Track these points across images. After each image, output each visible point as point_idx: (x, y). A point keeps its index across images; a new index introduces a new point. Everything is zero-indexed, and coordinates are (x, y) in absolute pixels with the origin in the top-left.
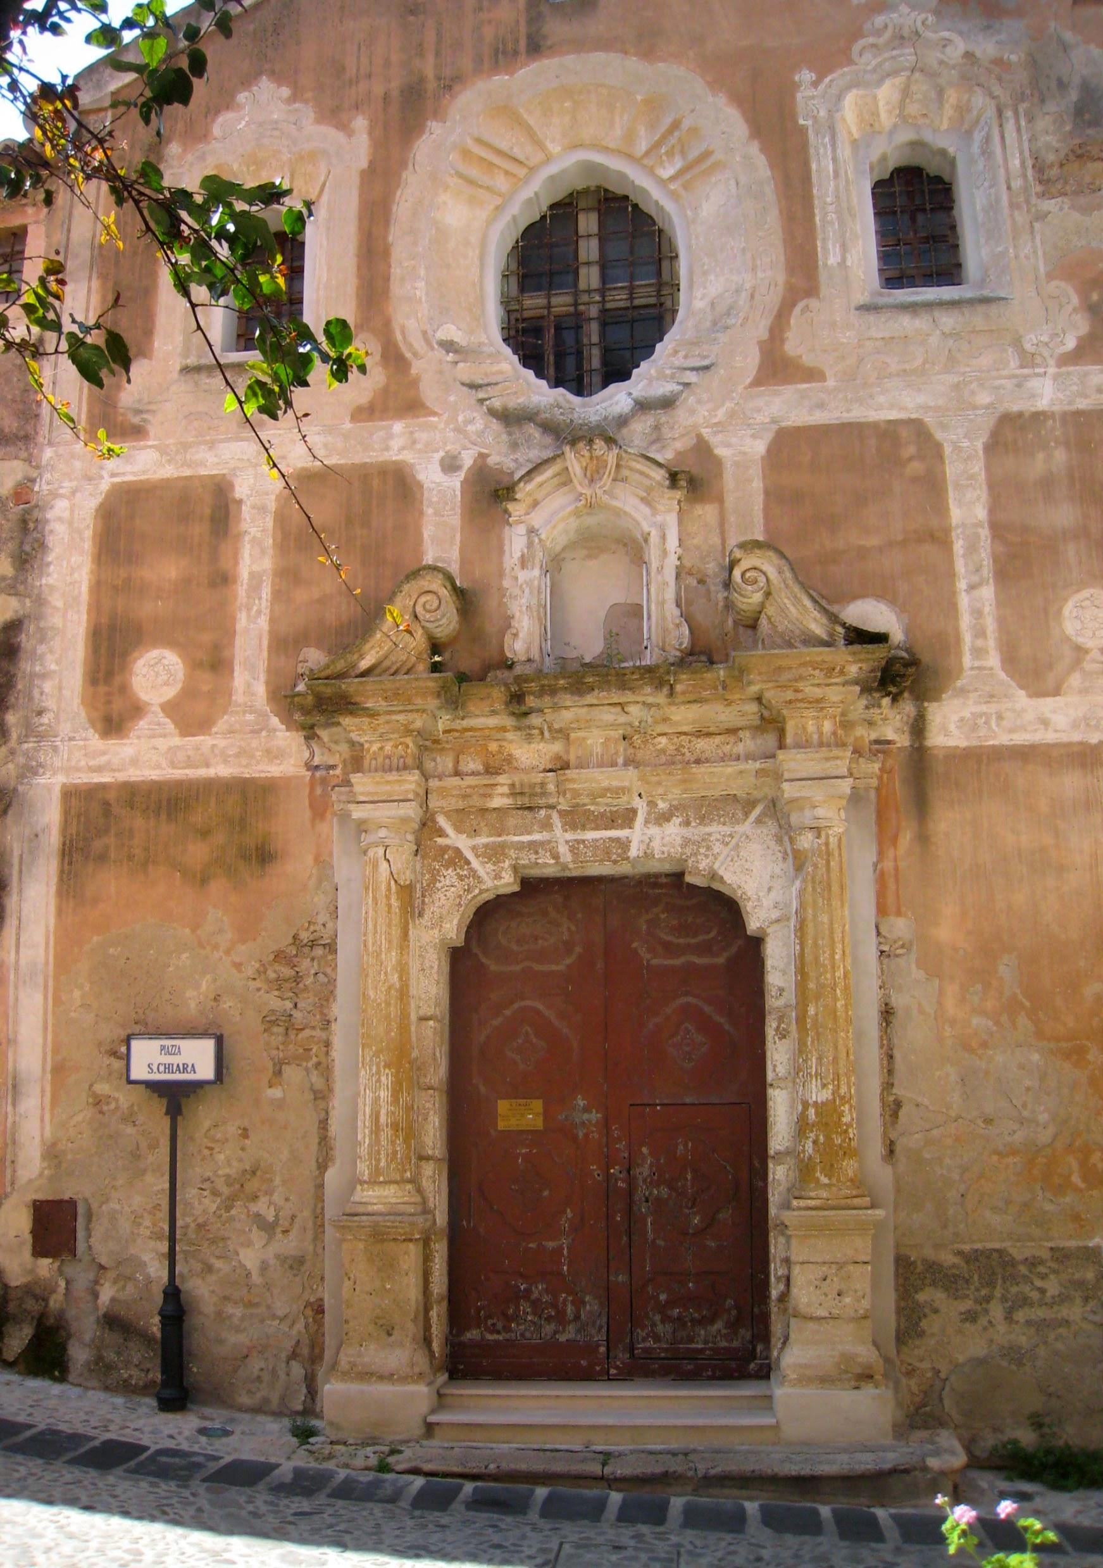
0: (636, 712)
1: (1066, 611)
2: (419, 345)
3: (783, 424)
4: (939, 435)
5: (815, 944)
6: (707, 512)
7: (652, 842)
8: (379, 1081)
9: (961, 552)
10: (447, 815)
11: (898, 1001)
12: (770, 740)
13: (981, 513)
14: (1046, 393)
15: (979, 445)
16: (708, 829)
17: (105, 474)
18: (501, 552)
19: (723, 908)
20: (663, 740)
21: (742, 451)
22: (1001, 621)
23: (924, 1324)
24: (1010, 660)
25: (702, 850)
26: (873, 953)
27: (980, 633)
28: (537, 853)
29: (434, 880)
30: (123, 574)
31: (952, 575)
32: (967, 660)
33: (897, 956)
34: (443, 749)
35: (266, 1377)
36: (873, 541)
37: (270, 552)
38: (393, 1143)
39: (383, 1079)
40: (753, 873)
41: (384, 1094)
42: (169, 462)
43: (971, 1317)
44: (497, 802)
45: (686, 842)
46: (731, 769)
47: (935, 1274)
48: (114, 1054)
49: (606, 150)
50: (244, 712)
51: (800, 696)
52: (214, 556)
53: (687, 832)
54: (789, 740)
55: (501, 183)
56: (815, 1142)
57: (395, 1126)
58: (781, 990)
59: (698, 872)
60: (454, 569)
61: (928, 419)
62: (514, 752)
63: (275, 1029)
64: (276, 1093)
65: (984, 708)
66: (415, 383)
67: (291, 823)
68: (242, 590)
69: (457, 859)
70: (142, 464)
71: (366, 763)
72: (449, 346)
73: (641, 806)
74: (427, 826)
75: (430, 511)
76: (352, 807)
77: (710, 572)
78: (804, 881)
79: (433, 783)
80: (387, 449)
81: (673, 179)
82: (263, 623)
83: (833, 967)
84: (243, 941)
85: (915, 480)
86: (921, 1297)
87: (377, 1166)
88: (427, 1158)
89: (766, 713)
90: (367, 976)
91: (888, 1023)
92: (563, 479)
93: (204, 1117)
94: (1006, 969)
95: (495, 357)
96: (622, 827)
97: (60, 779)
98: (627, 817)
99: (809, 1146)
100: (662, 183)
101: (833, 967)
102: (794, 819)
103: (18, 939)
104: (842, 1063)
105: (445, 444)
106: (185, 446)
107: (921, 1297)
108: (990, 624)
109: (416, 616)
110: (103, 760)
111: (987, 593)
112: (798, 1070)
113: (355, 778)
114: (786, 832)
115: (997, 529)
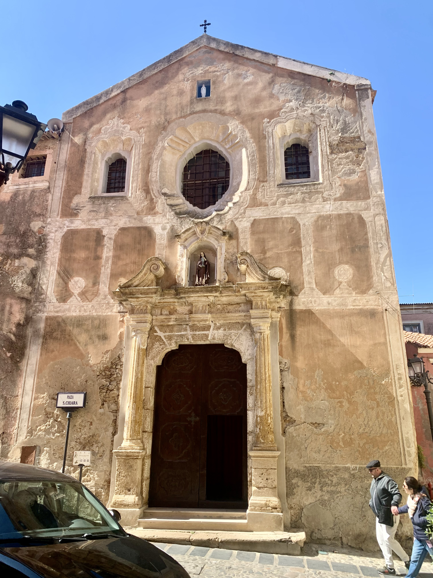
5: (260, 367)
6: (234, 242)
7: (214, 336)
10: (158, 326)
11: (285, 385)
12: (249, 306)
16: (231, 332)
17: (65, 226)
19: (235, 355)
20: (219, 306)
21: (243, 225)
25: (229, 338)
28: (182, 338)
29: (153, 345)
30: (68, 255)
33: (285, 371)
37: (112, 251)
38: (135, 427)
40: (242, 344)
42: (84, 224)
43: (309, 489)
45: (225, 335)
47: (297, 473)
48: (54, 399)
49: (211, 140)
51: (256, 295)
52: (96, 250)
53: (225, 333)
54: (253, 307)
55: (182, 148)
56: (259, 429)
58: (251, 380)
63: (103, 391)
64: (101, 411)
68: (103, 261)
69: (160, 339)
70: (78, 224)
71: (135, 311)
72: (165, 194)
74: (152, 329)
78: (257, 347)
81: (229, 148)
82: (109, 271)
86: (294, 481)
88: (145, 432)
89: (247, 299)
91: (283, 392)
92: (194, 233)
93: (78, 421)
94: (318, 373)
95: (178, 197)
96: (207, 331)
97: (46, 314)
98: (208, 328)
99: (258, 430)
100: (226, 149)
102: (255, 329)
103: (27, 363)
104: (268, 403)
106: (89, 220)
107: (294, 481)
110: (58, 309)
114: (253, 333)
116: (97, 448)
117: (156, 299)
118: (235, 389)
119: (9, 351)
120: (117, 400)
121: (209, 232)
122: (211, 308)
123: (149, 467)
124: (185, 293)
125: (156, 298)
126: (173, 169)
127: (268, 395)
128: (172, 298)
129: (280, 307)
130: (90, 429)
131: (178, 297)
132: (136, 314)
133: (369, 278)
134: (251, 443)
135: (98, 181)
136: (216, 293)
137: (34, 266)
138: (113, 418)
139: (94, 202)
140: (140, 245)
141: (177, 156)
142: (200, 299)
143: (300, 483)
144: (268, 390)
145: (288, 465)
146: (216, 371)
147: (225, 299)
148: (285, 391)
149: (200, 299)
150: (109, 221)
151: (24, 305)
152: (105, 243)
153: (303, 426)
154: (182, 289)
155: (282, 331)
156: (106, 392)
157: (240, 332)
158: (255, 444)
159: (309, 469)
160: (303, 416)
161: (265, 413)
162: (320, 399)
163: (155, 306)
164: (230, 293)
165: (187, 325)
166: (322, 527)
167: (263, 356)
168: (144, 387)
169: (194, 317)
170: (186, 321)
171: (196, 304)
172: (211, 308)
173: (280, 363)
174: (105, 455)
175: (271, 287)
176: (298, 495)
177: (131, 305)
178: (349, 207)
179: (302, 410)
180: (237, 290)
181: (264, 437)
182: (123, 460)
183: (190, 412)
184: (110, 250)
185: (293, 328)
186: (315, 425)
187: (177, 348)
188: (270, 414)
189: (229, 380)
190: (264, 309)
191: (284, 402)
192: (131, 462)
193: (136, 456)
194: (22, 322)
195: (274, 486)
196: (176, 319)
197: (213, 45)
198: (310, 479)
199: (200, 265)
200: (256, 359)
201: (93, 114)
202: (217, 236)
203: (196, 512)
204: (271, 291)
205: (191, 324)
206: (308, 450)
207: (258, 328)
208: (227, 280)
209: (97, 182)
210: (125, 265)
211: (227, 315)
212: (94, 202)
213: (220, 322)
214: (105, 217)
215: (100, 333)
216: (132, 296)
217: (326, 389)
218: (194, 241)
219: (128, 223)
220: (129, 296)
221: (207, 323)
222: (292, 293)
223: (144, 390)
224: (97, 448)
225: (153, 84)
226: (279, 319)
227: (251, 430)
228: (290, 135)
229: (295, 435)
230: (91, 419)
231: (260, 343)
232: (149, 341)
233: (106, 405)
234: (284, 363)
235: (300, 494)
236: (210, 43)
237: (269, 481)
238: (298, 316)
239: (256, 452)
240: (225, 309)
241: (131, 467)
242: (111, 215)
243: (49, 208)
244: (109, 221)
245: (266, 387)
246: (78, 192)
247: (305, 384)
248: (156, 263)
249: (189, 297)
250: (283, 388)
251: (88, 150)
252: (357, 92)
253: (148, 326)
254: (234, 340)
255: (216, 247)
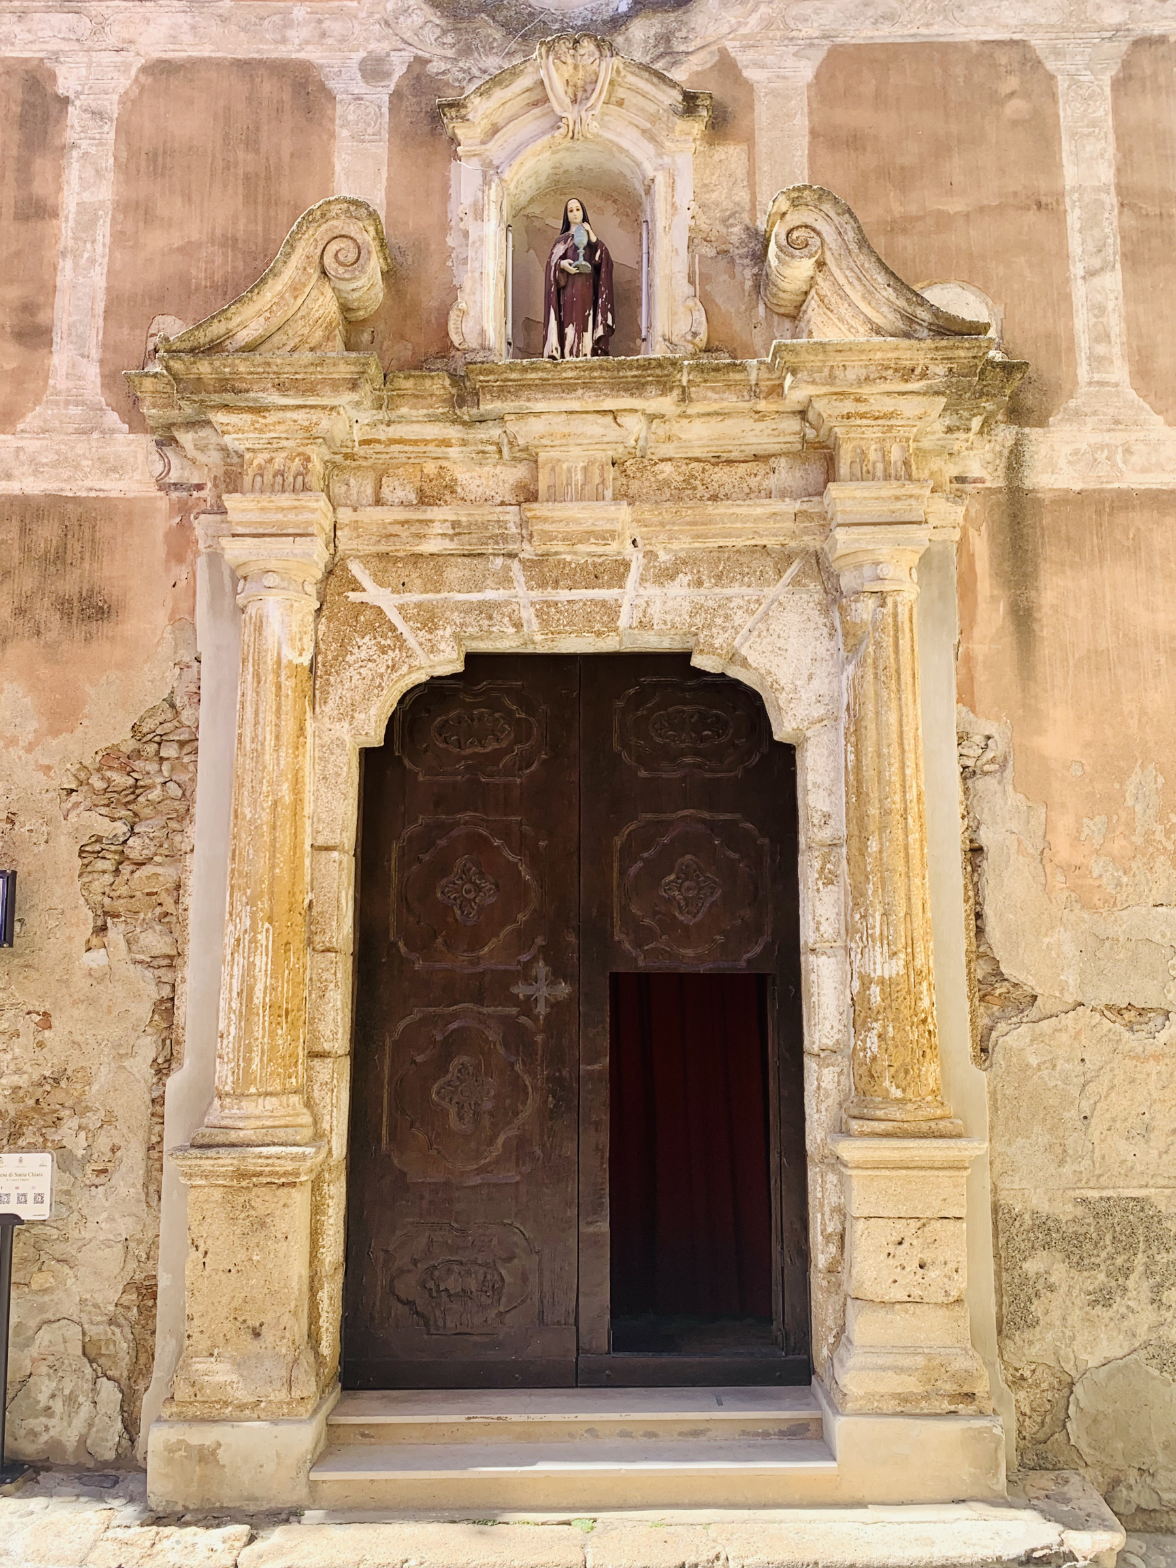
0: (634, 426)
3: (839, 40)
4: (1051, 65)
6: (731, 154)
7: (644, 615)
8: (254, 941)
9: (1077, 226)
10: (365, 559)
11: (985, 838)
12: (815, 472)
13: (1106, 174)
15: (1106, 80)
16: (727, 592)
18: (445, 197)
20: (667, 468)
23: (1037, 1308)
24: (1143, 371)
25: (719, 621)
28: (491, 618)
31: (1063, 256)
33: (986, 774)
34: (359, 467)
35: (58, 1406)
36: (956, 206)
38: (272, 1034)
39: (261, 937)
40: (784, 659)
41: (261, 962)
43: (1102, 1298)
44: (430, 546)
45: (697, 609)
46: (761, 508)
47: (1046, 1232)
50: (67, 403)
51: (862, 408)
53: (699, 595)
54: (844, 469)
59: (712, 650)
60: (378, 199)
61: (1038, 42)
62: (459, 477)
63: (100, 865)
64: (97, 958)
65: (1107, 438)
67: (133, 567)
68: (66, 228)
69: (378, 622)
71: (247, 480)
73: (636, 559)
74: (334, 573)
75: (345, 133)
76: (224, 542)
77: (734, 239)
79: (345, 515)
80: (284, 41)
83: (903, 786)
84: (55, 732)
86: (1030, 1267)
87: (247, 1071)
89: (811, 434)
90: (241, 786)
91: (975, 867)
98: (617, 572)
101: (903, 786)
104: (918, 921)
105: (367, 40)
107: (1030, 1267)
108: (1116, 325)
109: (324, 273)
111: (1113, 281)
112: (850, 930)
113: (231, 501)
114: (835, 597)
116: (82, 1134)
117: (350, 417)
118: (736, 856)
120: (169, 907)
121: (610, 94)
122: (627, 475)
123: (342, 1213)
124: (502, 392)
125: (354, 414)
127: (917, 881)
128: (433, 419)
129: (961, 480)
130: (41, 1045)
131: (466, 413)
132: (252, 490)
134: (830, 1101)
136: (663, 393)
138: (153, 993)
140: (257, 151)
142: (578, 425)
143: (1059, 1273)
144: (916, 862)
145: (1005, 1198)
146: (643, 774)
147: (699, 435)
148: (985, 864)
149: (573, 424)
150: (84, 25)
152: (70, 136)
153: (1070, 1023)
154: (491, 372)
155: (974, 590)
156: (117, 872)
157: (770, 592)
158: (858, 1109)
159: (1102, 1211)
160: (1071, 978)
161: (907, 966)
162: (1151, 903)
163: (344, 461)
164: (731, 401)
165: (511, 555)
166: (1161, 1458)
167: (894, 704)
168: (308, 848)
169: (546, 520)
170: (505, 538)
171: (555, 454)
172: (627, 475)
173: (962, 738)
174: (123, 1169)
175: (941, 370)
176: (1050, 1325)
177: (224, 449)
179: (1070, 950)
180: (765, 386)
182: (217, 1194)
183: (525, 958)
184: (98, 173)
185: (1025, 575)
186: (1127, 1015)
187: (459, 667)
188: (925, 971)
189: (706, 815)
190: (897, 479)
191: (978, 916)
192: (264, 1202)
193: (285, 1174)
195: (954, 1294)
196: (455, 524)
198: (1104, 1255)
199: (565, 263)
200: (855, 724)
202: (654, 119)
203: (583, 1417)
204: (937, 393)
205: (528, 551)
206: (1098, 1125)
207: (867, 571)
210: (181, 250)
211: (710, 508)
213: (676, 546)
215: (69, 585)
216: (228, 397)
218: (534, 138)
219: (188, 38)
220: (216, 398)
221: (614, 547)
222: (1017, 414)
223: (307, 862)
224: (82, 1134)
226: (956, 535)
227: (830, 1043)
229: (1034, 1061)
230: (42, 998)
231: (878, 645)
232: (322, 628)
233: (116, 933)
234: (978, 739)
235: (1058, 1323)
237: (933, 1274)
238: (1047, 520)
239: (875, 1143)
240: (697, 483)
241: (263, 1224)
245: (906, 848)
247: (1079, 832)
248: (353, 229)
249: (520, 415)
250: (975, 851)
253: (318, 553)
254: (744, 631)
255: (650, 173)
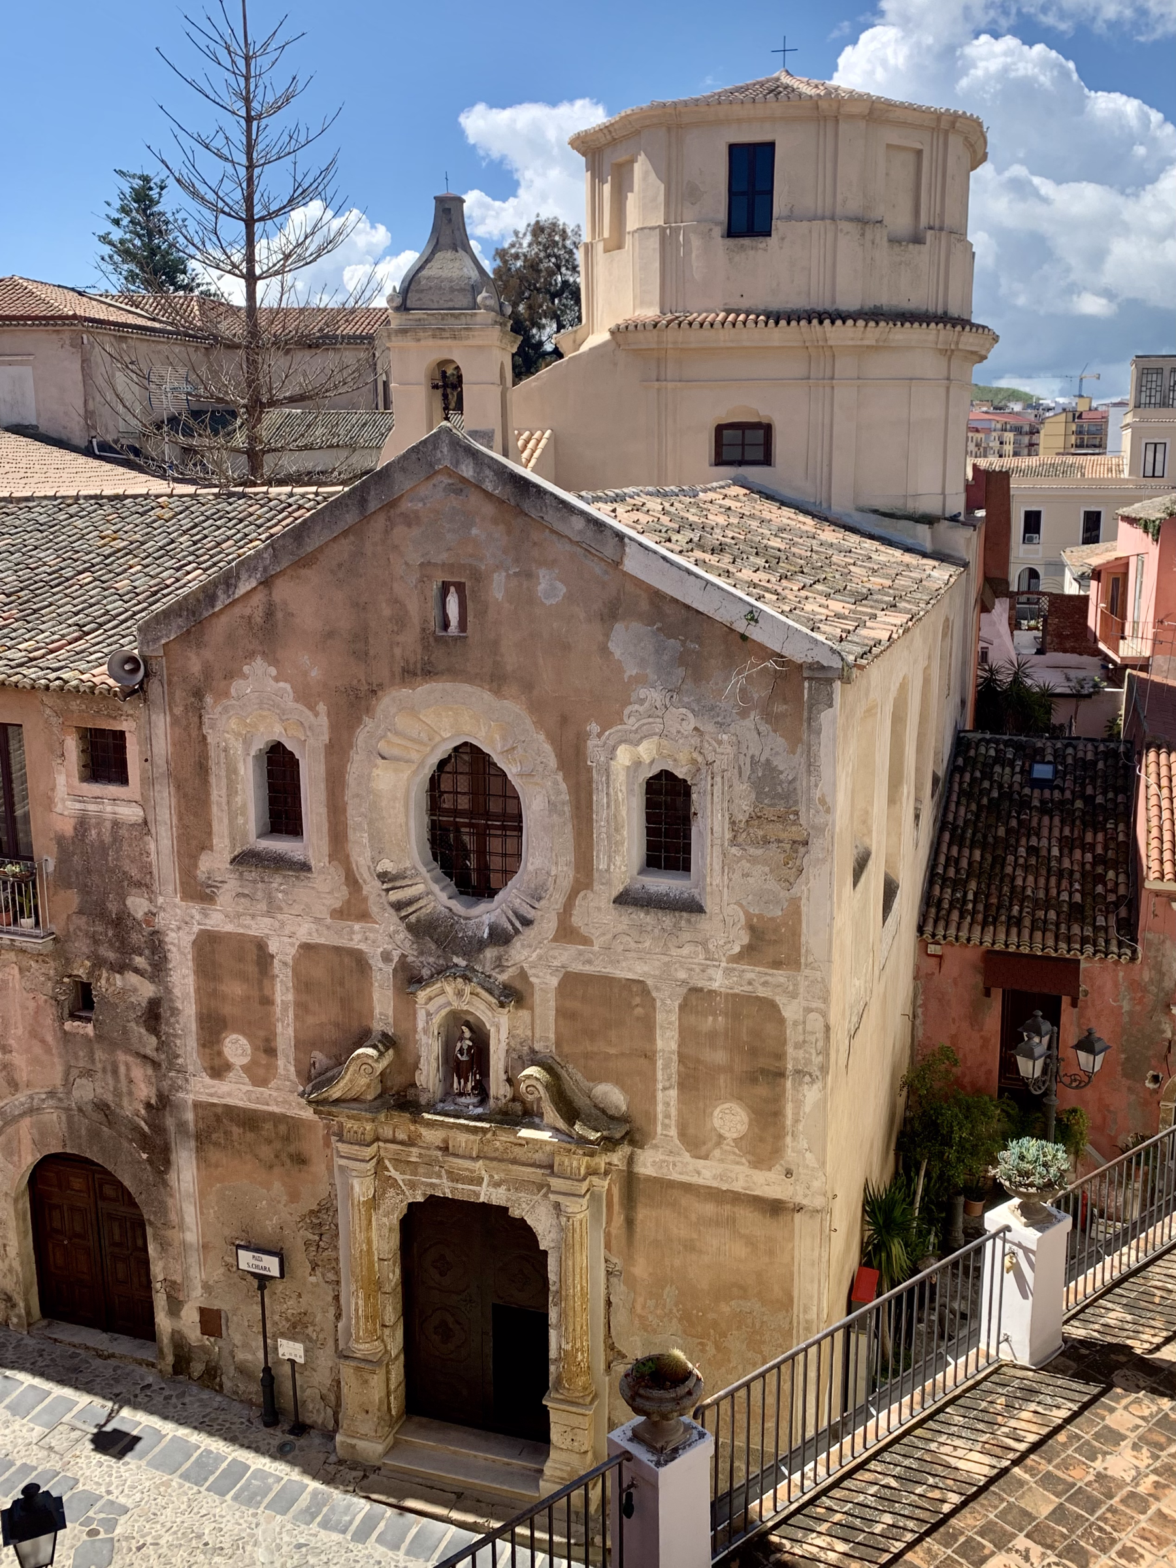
1: (716, 1113)
2: (366, 875)
4: (654, 994)
6: (524, 1014)
13: (674, 1046)
14: (718, 981)
15: (677, 1004)
21: (544, 983)
22: (680, 1111)
24: (682, 1135)
26: (603, 1274)
27: (667, 1116)
31: (655, 1080)
32: (659, 1129)
36: (612, 1051)
52: (260, 982)
57: (367, 1318)
61: (650, 982)
64: (313, 1279)
66: (365, 900)
69: (395, 1184)
82: (291, 1031)
85: (638, 1019)
94: (670, 1293)
106: (239, 915)
108: (673, 1112)
110: (212, 1090)
111: (674, 1093)
115: (682, 1058)
119: (144, 1150)
126: (400, 806)
133: (779, 1136)
135: (243, 810)
137: (151, 994)
139: (241, 874)
141: (405, 775)
151: (150, 1072)
178: (754, 979)
181: (569, 1380)
194: (153, 1102)
197: (467, 470)
201: (206, 638)
208: (509, 1096)
209: (243, 814)
212: (241, 874)
214: (269, 914)
215: (292, 1149)
217: (680, 1320)
225: (332, 571)
228: (652, 762)
236: (457, 463)
242: (280, 909)
243: (155, 872)
244: (277, 925)
246: (206, 846)
250: (609, 1303)
251: (209, 740)
252: (806, 684)
